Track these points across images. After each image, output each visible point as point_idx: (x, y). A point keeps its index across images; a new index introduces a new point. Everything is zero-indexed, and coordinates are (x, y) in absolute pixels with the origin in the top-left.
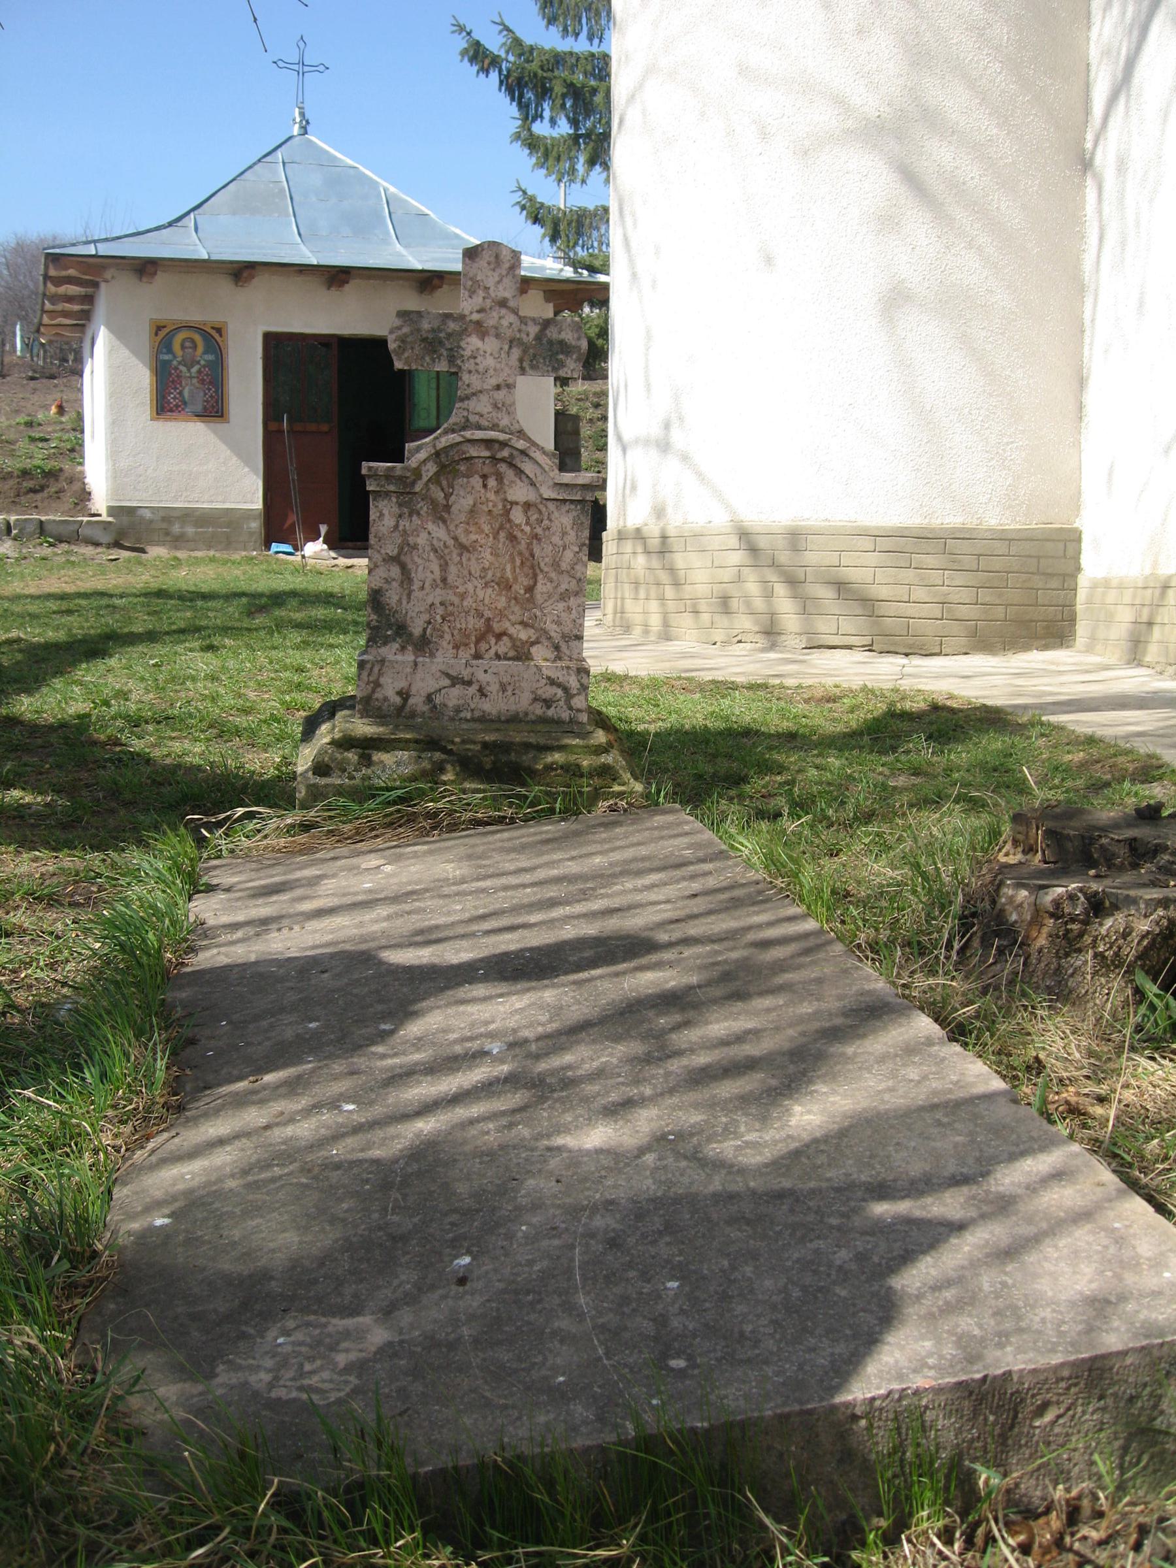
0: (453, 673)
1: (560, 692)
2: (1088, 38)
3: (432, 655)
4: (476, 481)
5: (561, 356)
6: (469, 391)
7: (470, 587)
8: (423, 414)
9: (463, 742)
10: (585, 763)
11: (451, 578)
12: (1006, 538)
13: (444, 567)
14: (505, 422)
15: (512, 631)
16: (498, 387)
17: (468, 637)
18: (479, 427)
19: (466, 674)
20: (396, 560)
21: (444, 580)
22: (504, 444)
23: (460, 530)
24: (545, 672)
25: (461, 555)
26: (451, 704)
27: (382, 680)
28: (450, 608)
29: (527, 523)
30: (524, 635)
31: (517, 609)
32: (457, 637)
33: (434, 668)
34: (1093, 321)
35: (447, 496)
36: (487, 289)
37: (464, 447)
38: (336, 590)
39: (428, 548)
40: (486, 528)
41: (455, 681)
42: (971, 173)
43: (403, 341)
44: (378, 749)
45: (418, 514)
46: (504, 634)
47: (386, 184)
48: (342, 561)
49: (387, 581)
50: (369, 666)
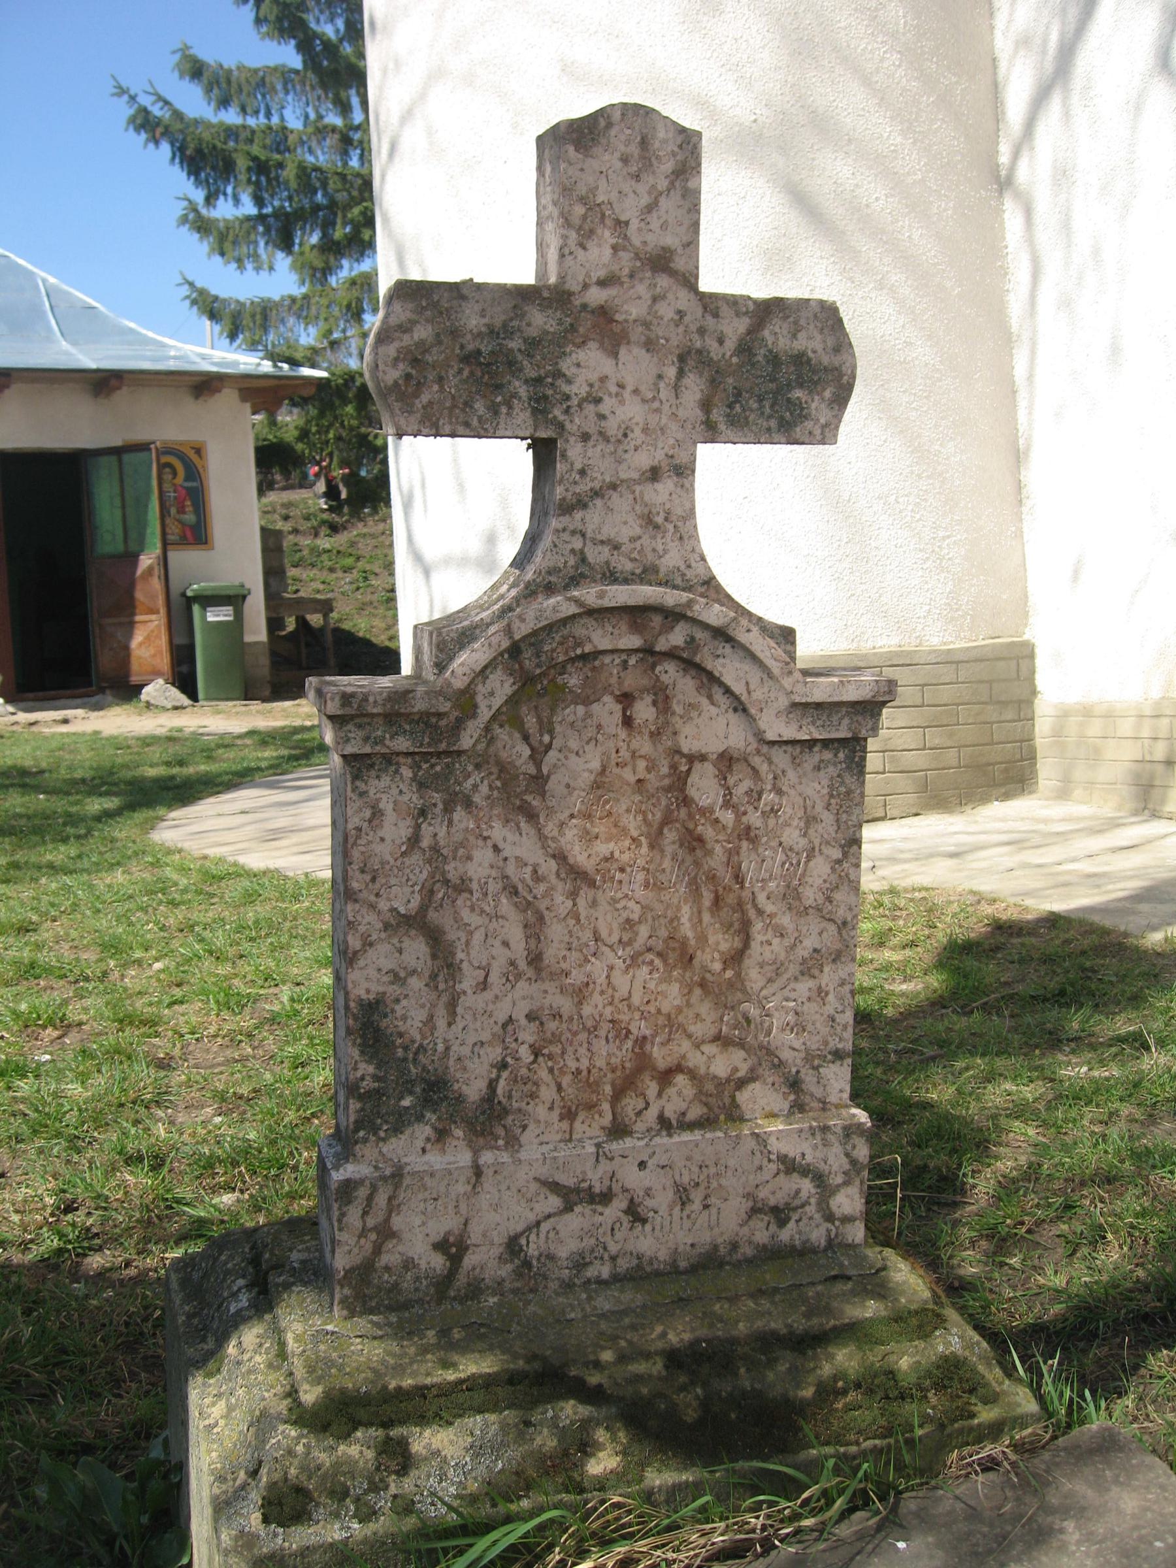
0: (567, 1180)
1: (807, 1186)
2: (992, 28)
3: (513, 1143)
4: (607, 711)
5: (798, 394)
6: (584, 487)
7: (598, 968)
8: (108, 537)
9: (622, 1358)
10: (904, 1363)
11: (552, 954)
12: (951, 660)
13: (535, 927)
14: (671, 560)
15: (695, 1060)
16: (654, 474)
17: (594, 1087)
18: (612, 576)
19: (596, 1178)
20: (415, 923)
21: (535, 960)
22: (673, 616)
23: (570, 834)
24: (775, 1145)
25: (573, 895)
26: (563, 1253)
27: (397, 1222)
28: (552, 1026)
29: (727, 804)
30: (722, 1064)
31: (705, 1008)
32: (570, 1091)
33: (523, 1176)
34: (1030, 378)
35: (537, 756)
36: (620, 225)
37: (579, 630)
38: (28, 763)
39: (493, 887)
40: (633, 824)
41: (572, 1197)
42: (876, 195)
43: (415, 362)
44: (423, 1420)
45: (468, 804)
46: (679, 1069)
47: (43, 274)
48: (23, 717)
49: (396, 978)
50: (363, 1192)
